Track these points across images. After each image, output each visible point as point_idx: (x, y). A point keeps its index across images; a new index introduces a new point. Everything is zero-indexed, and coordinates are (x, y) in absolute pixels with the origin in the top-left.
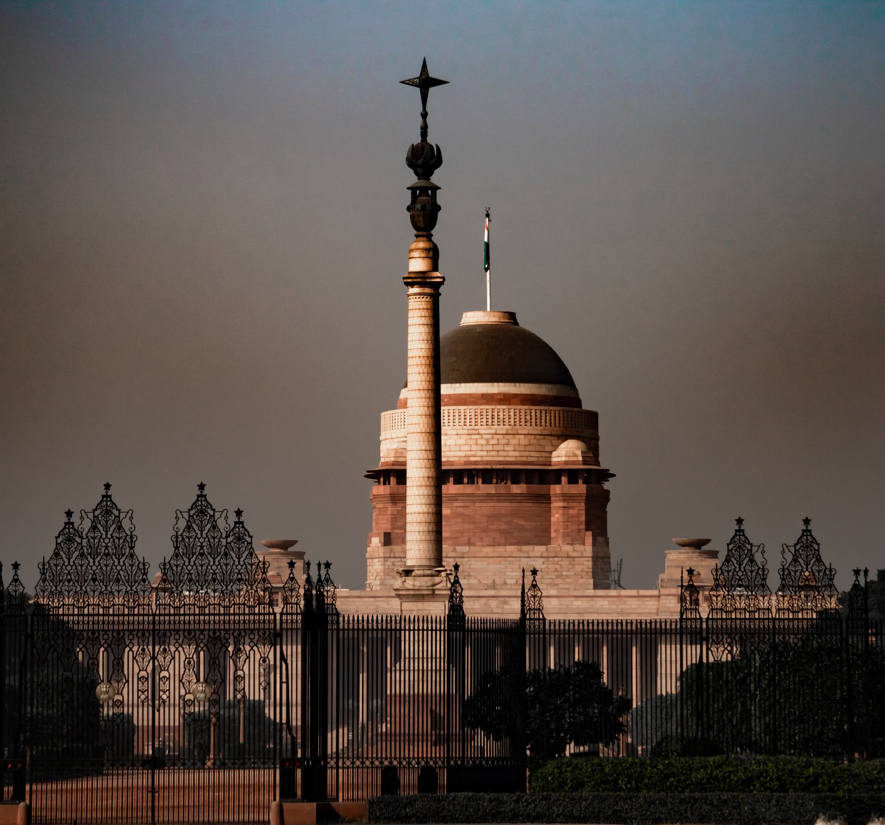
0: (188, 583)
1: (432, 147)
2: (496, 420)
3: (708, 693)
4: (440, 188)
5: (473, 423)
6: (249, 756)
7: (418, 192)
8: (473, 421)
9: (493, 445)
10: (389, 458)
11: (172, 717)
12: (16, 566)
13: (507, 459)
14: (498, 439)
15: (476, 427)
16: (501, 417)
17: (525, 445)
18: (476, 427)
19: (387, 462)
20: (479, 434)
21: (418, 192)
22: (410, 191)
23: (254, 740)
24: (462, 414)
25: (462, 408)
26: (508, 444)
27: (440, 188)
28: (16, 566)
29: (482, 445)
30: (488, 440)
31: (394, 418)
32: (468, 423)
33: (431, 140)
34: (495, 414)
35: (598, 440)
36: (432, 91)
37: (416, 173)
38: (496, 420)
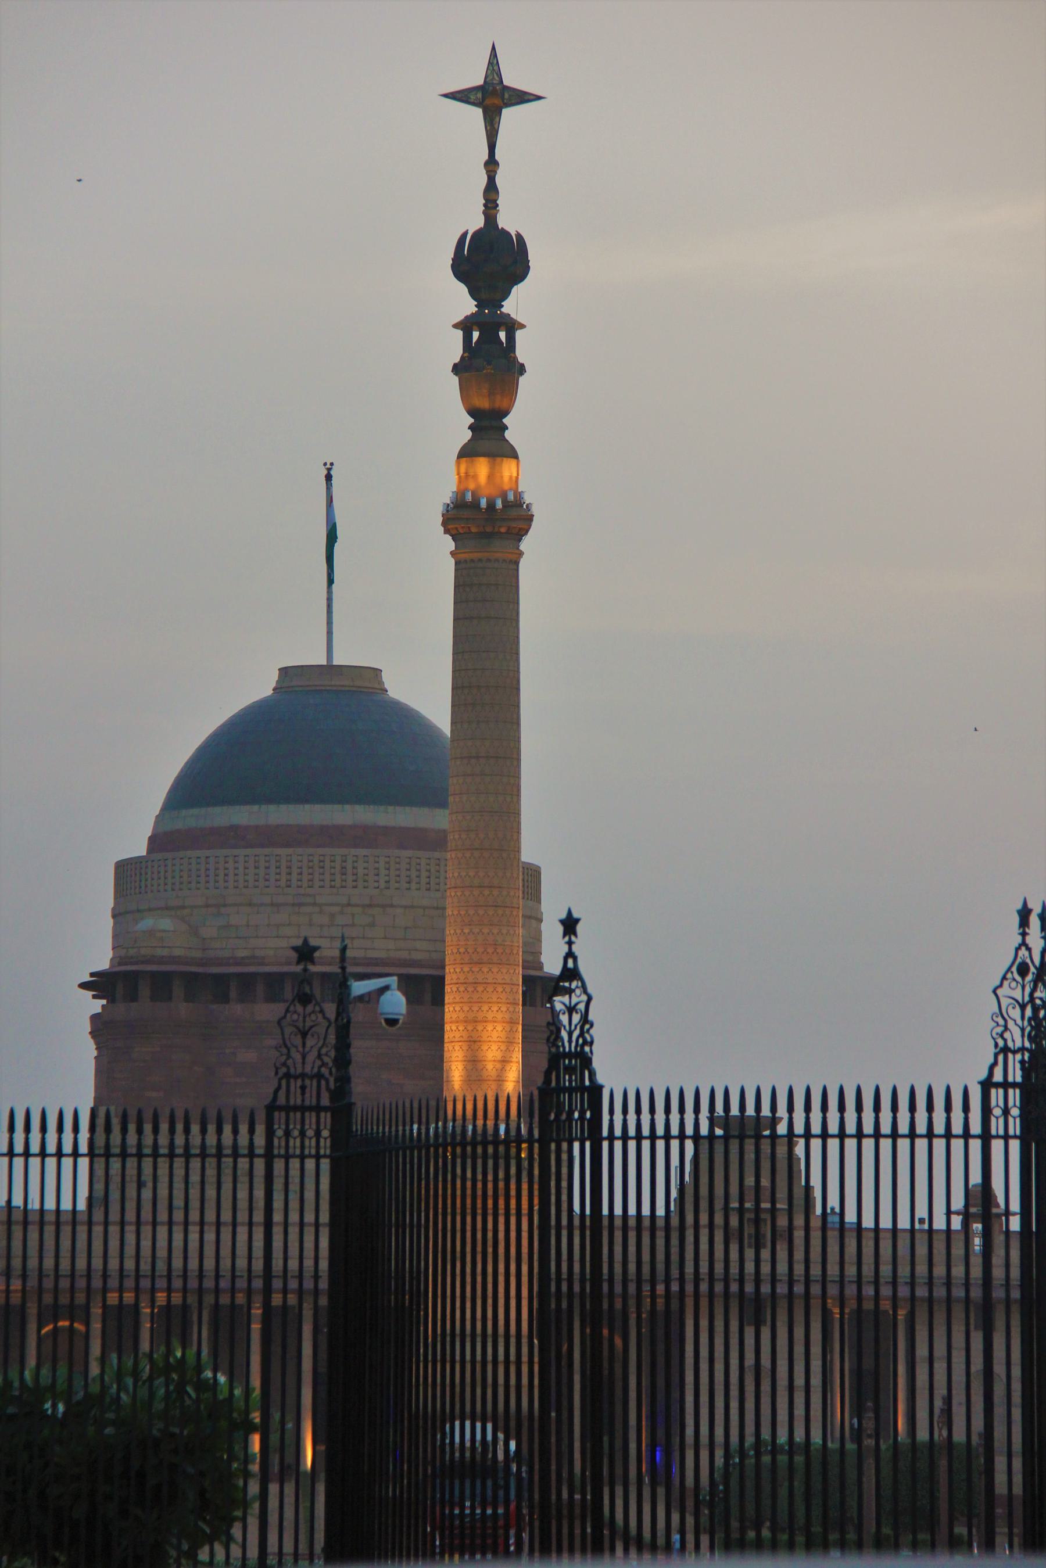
0: (1019, 979)
1: (508, 234)
2: (350, 878)
3: (434, 1467)
4: (522, 326)
5: (305, 884)
6: (774, 1461)
7: (476, 335)
8: (305, 877)
9: (343, 926)
10: (135, 950)
11: (719, 1341)
12: (570, 925)
13: (372, 954)
14: (353, 915)
15: (310, 891)
16: (361, 871)
17: (406, 928)
18: (310, 891)
19: (132, 957)
20: (314, 904)
21: (476, 335)
22: (459, 334)
23: (611, 1112)
24: (284, 864)
25: (283, 852)
26: (372, 925)
27: (522, 326)
28: (570, 925)
29: (321, 926)
30: (332, 916)
31: (143, 872)
32: (294, 883)
33: (506, 221)
34: (349, 865)
35: (541, 921)
36: (508, 114)
37: (473, 293)
38: (350, 878)
